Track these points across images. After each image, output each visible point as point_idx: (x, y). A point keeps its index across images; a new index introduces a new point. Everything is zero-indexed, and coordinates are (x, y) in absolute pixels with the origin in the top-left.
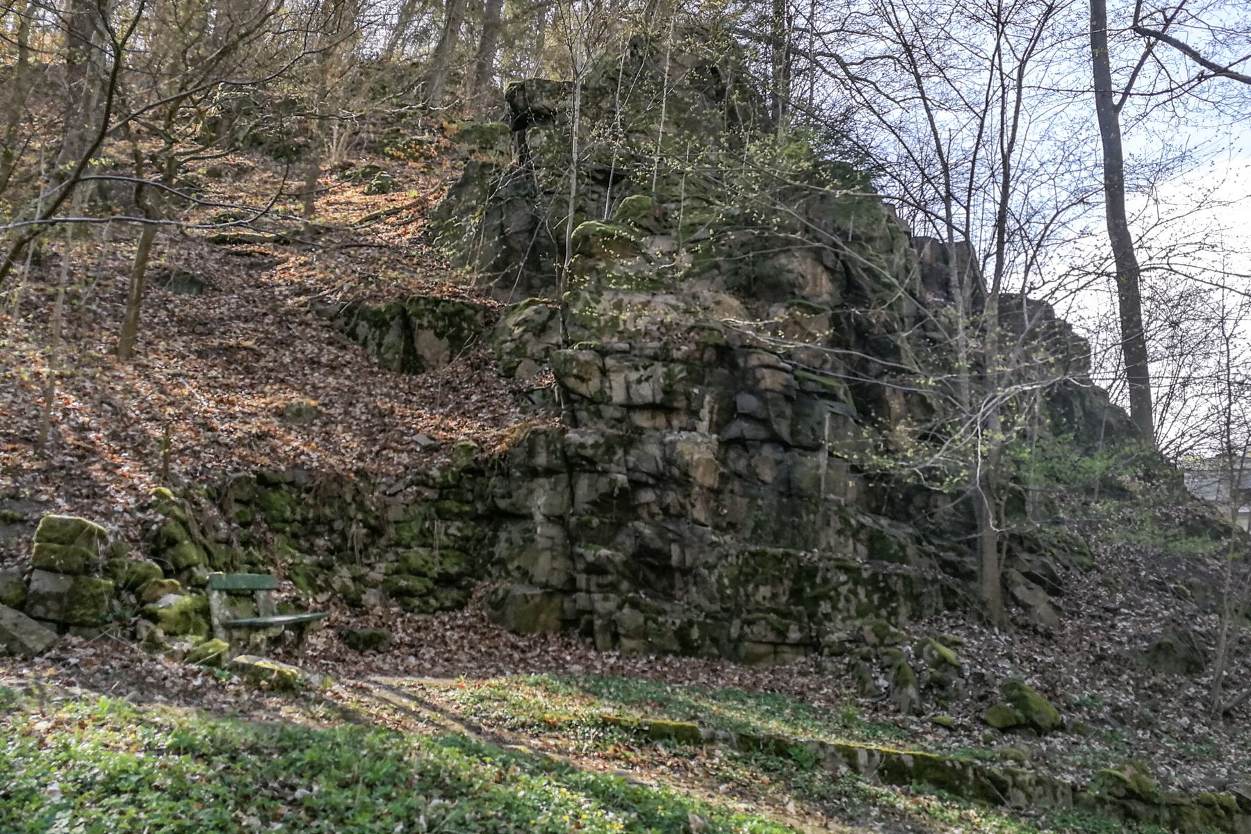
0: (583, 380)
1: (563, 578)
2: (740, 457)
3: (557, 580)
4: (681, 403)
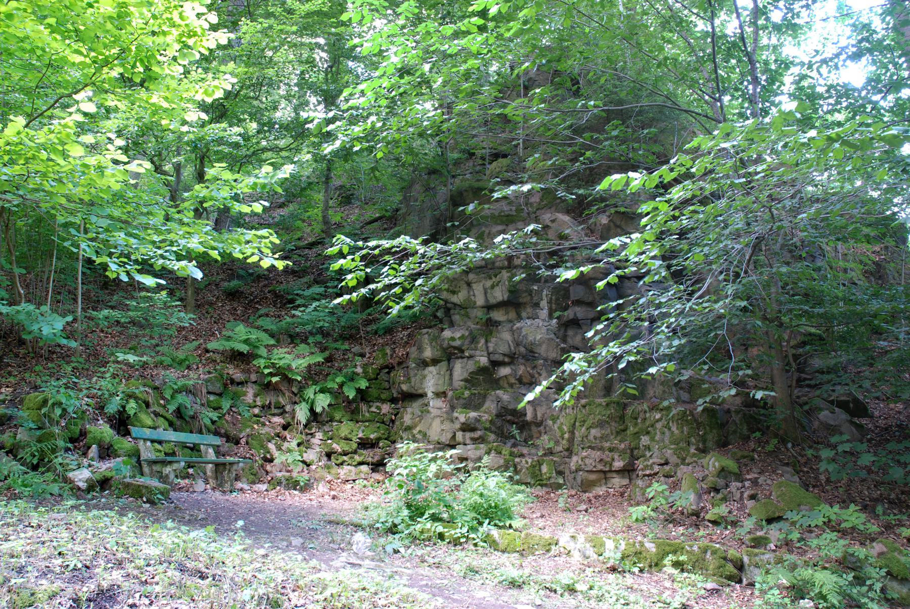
0: (454, 292)
1: (449, 435)
4: (524, 298)
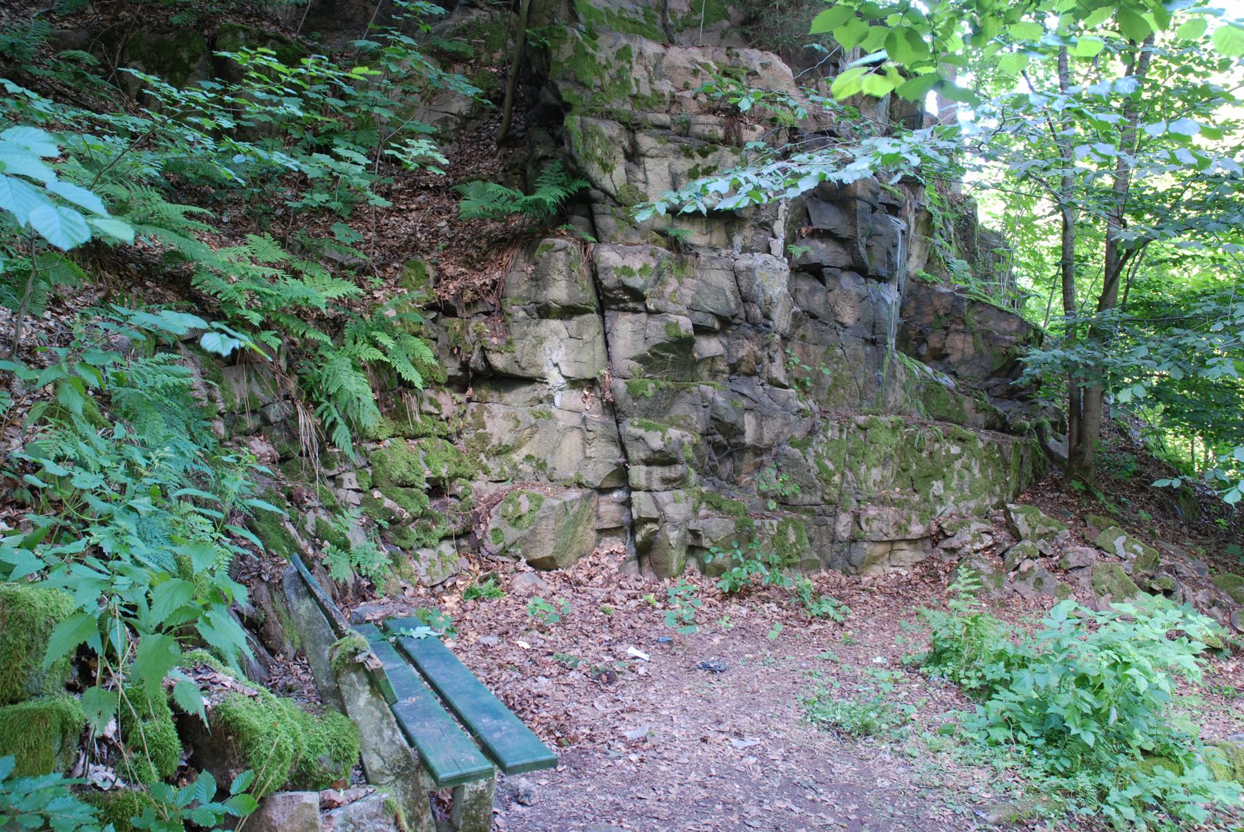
2: (813, 291)
3: (597, 472)
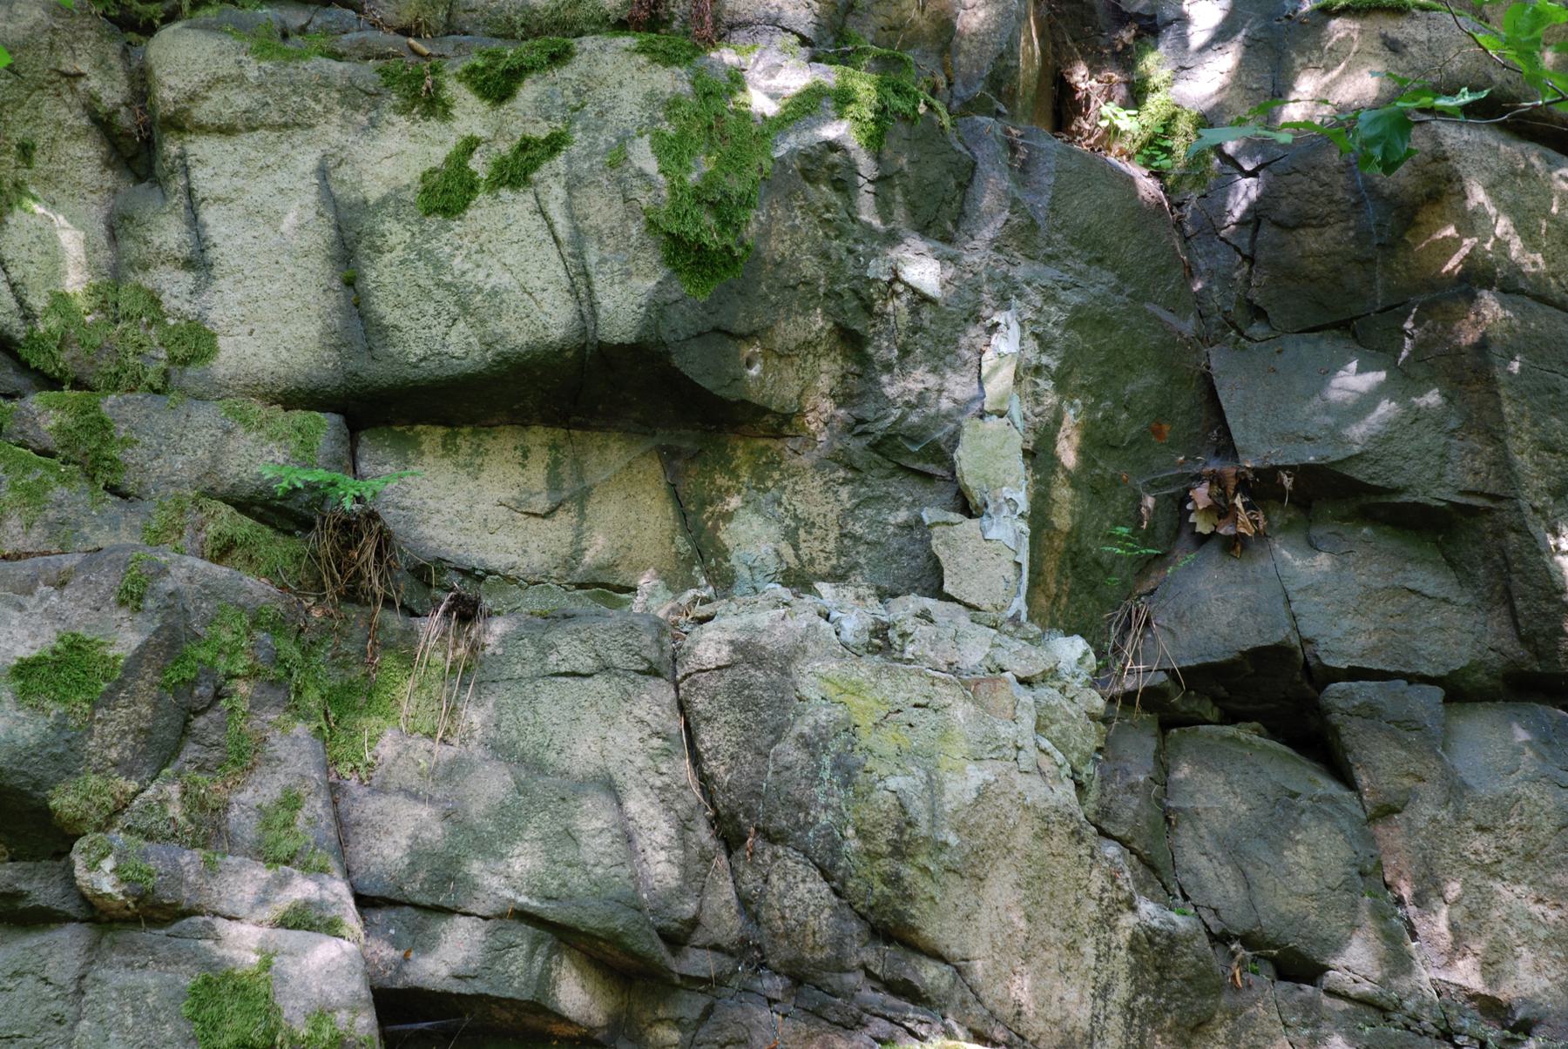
2: (1283, 811)
